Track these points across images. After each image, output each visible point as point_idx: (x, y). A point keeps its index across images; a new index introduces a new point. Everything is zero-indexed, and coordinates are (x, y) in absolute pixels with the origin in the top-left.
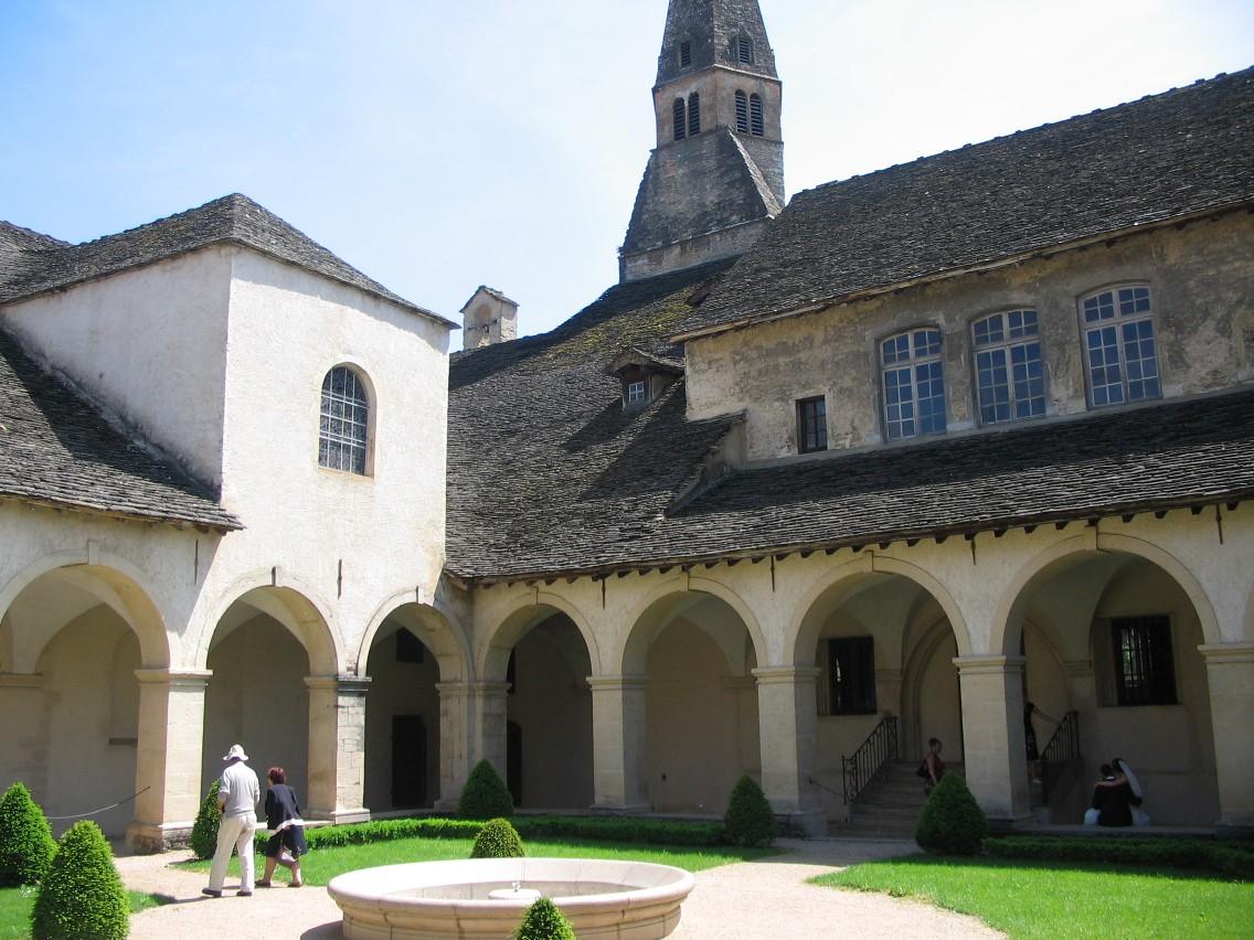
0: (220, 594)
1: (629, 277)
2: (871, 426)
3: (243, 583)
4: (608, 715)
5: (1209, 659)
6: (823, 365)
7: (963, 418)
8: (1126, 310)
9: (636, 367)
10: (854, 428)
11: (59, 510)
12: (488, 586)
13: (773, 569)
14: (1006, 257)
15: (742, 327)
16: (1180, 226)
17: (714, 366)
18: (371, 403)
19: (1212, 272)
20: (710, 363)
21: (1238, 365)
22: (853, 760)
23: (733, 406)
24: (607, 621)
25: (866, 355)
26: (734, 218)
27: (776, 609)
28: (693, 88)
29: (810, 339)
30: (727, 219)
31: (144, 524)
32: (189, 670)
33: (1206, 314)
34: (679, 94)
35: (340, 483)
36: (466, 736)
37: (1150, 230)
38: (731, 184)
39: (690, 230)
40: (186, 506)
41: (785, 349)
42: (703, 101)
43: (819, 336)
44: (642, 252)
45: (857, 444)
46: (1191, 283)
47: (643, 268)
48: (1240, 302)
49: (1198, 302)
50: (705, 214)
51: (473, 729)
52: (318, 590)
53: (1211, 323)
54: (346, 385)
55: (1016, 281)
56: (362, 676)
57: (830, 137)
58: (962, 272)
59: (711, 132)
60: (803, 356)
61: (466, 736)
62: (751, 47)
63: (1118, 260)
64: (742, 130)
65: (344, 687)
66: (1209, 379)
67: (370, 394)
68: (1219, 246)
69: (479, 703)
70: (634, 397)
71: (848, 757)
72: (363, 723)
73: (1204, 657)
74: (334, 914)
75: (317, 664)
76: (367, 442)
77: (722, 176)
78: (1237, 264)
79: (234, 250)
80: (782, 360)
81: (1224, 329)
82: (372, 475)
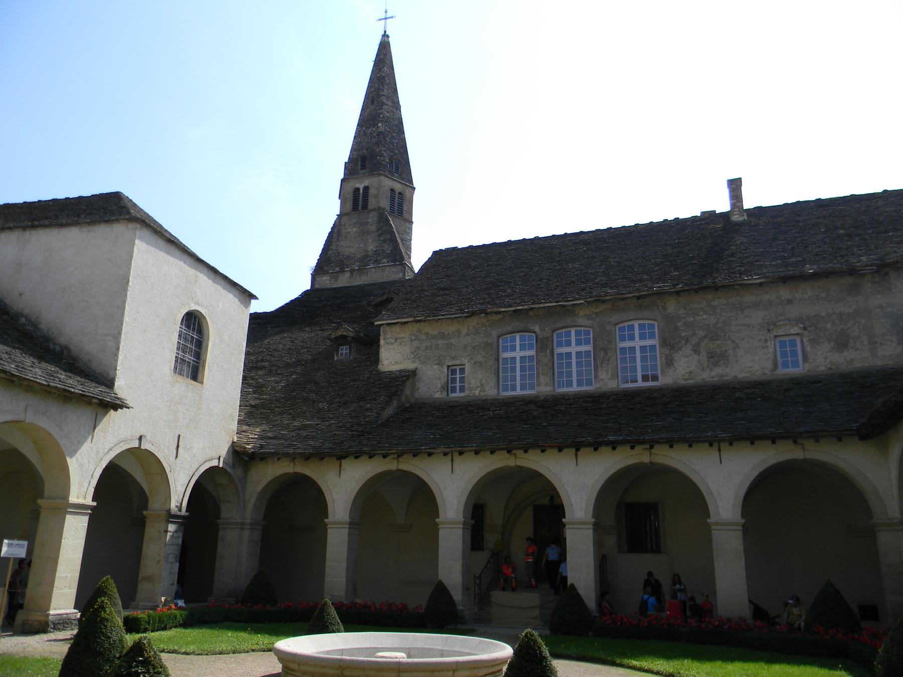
0: (106, 451)
1: (317, 286)
2: (492, 384)
3: (122, 444)
4: (337, 543)
5: (713, 527)
6: (465, 347)
7: (546, 385)
8: (642, 337)
9: (345, 337)
10: (482, 385)
11: (13, 382)
12: (262, 459)
13: (452, 461)
14: (579, 299)
15: (420, 321)
16: (678, 293)
17: (398, 341)
18: (205, 338)
19: (691, 319)
20: (396, 339)
21: (703, 370)
22: (480, 577)
23: (409, 365)
24: (341, 486)
25: (491, 344)
26: (384, 260)
27: (453, 482)
28: (366, 183)
29: (459, 332)
30: (380, 261)
31: (66, 397)
32: (81, 501)
33: (687, 341)
34: (357, 185)
35: (184, 384)
36: (236, 556)
37: (661, 294)
38: (385, 241)
39: (357, 264)
40: (94, 390)
41: (442, 336)
42: (372, 191)
43: (464, 331)
44: (325, 273)
45: (482, 394)
46: (679, 324)
47: (326, 281)
48: (705, 337)
49: (683, 334)
50: (367, 256)
51: (245, 554)
52: (165, 455)
53: (689, 347)
54: (194, 322)
55: (582, 313)
56: (184, 512)
57: (437, 226)
58: (554, 304)
59: (374, 210)
60: (453, 341)
61: (236, 556)
62: (400, 166)
63: (640, 307)
64: (392, 212)
65: (170, 517)
66: (687, 376)
67: (205, 330)
68: (695, 306)
69: (247, 533)
70: (342, 354)
71: (477, 575)
72: (180, 543)
73: (710, 526)
74: (278, 668)
75: (155, 504)
76: (201, 362)
77: (379, 235)
78: (705, 317)
79: (138, 226)
80: (441, 342)
81: (696, 351)
82: (202, 383)
